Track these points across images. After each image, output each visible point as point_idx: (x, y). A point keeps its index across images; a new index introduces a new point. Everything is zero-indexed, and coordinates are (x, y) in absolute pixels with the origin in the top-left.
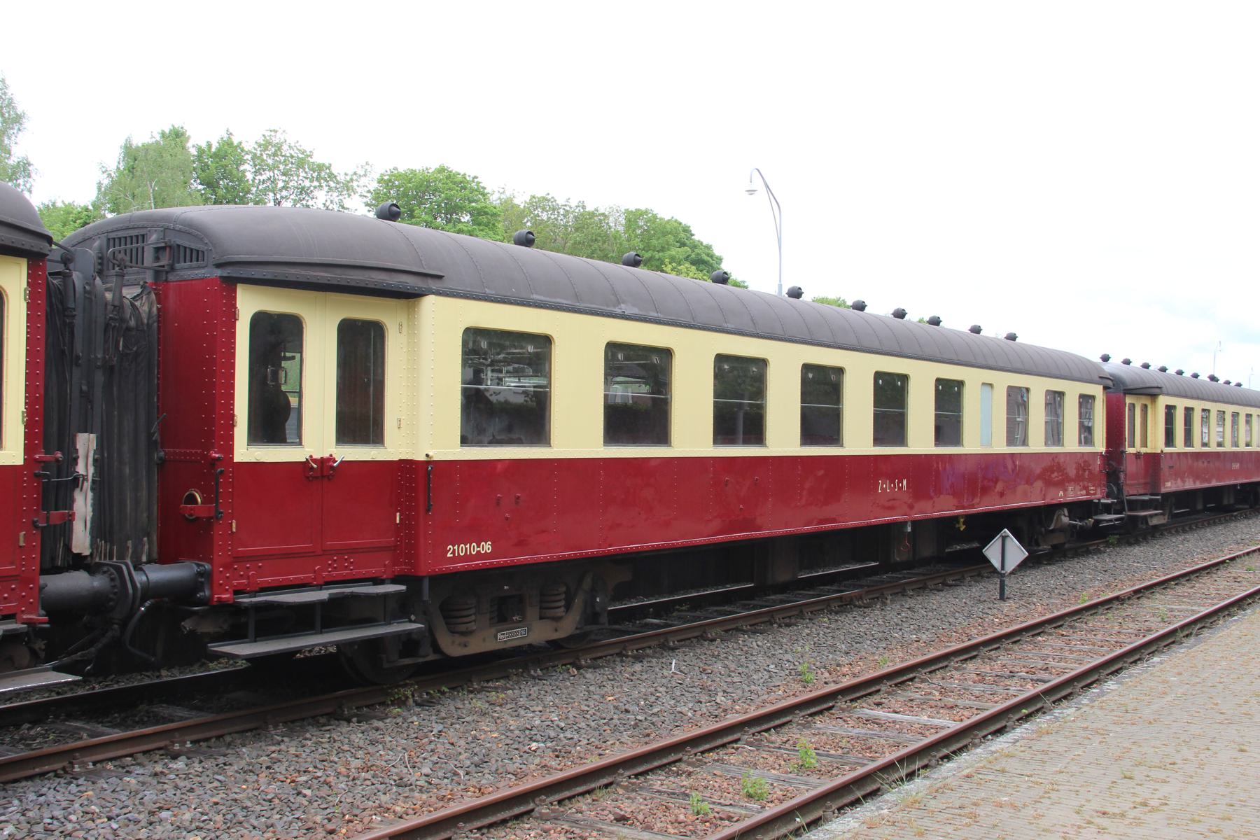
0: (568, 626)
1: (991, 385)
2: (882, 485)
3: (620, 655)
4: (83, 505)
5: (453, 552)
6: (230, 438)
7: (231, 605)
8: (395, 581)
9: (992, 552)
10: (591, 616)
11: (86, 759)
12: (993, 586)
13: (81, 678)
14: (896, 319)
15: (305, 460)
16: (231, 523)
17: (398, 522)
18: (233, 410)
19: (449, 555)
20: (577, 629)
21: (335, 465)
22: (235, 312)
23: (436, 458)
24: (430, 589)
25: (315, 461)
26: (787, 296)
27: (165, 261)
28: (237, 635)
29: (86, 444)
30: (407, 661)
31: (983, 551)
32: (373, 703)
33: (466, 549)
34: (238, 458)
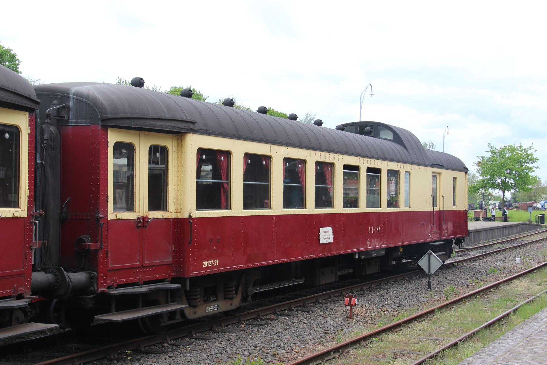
0: (236, 302)
1: (409, 172)
2: (370, 229)
3: (256, 319)
8: (173, 281)
9: (423, 263)
10: (244, 299)
12: (425, 281)
13: (57, 325)
14: (338, 131)
20: (239, 304)
26: (336, 129)
30: (171, 322)
31: (418, 262)
32: (235, 322)
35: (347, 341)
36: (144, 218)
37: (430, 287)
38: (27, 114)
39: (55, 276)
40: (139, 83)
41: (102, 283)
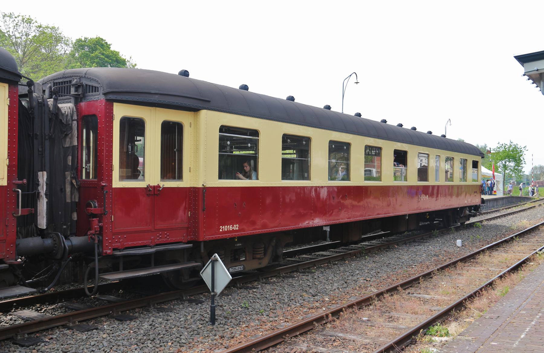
4: (43, 205)
5: (223, 229)
6: (111, 176)
7: (112, 255)
8: (188, 243)
10: (275, 258)
11: (75, 320)
15: (146, 187)
16: (111, 217)
17: (189, 216)
18: (112, 162)
19: (221, 230)
20: (269, 263)
21: (161, 189)
22: (113, 116)
23: (207, 186)
24: (204, 246)
25: (151, 187)
27: (80, 91)
28: (115, 269)
29: (43, 177)
33: (228, 228)
34: (114, 186)
35: (253, 340)
36: (154, 187)
37: (213, 320)
38: (6, 86)
39: (54, 241)
40: (185, 73)
41: (107, 246)
